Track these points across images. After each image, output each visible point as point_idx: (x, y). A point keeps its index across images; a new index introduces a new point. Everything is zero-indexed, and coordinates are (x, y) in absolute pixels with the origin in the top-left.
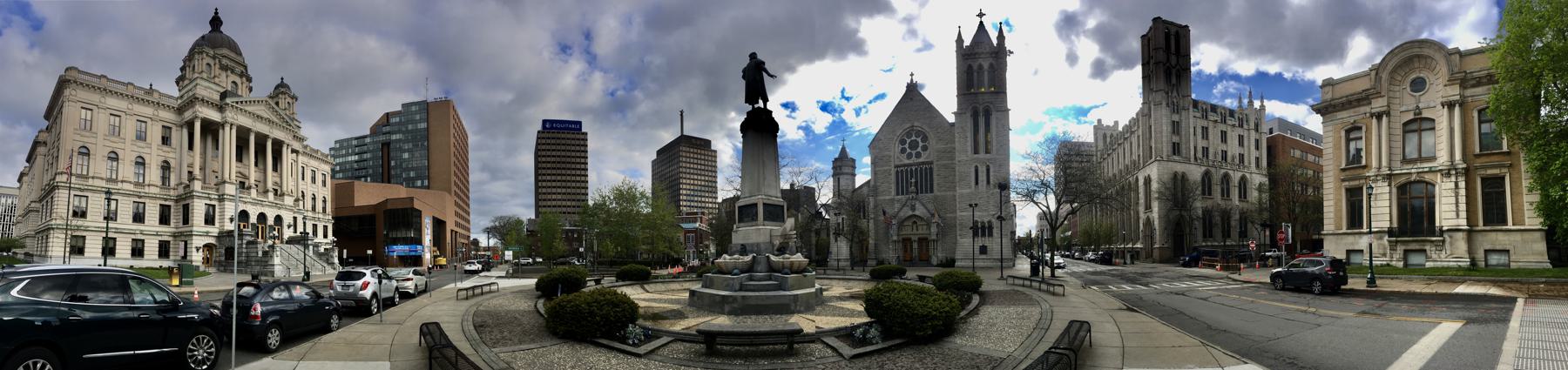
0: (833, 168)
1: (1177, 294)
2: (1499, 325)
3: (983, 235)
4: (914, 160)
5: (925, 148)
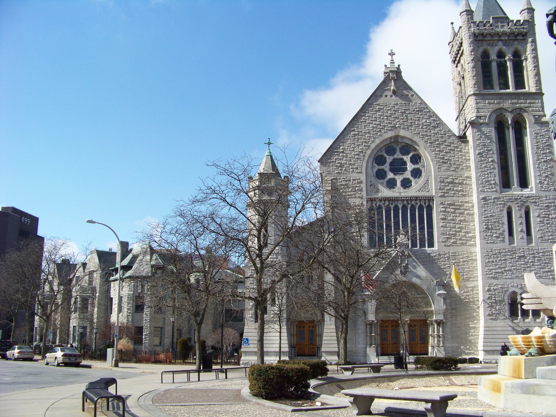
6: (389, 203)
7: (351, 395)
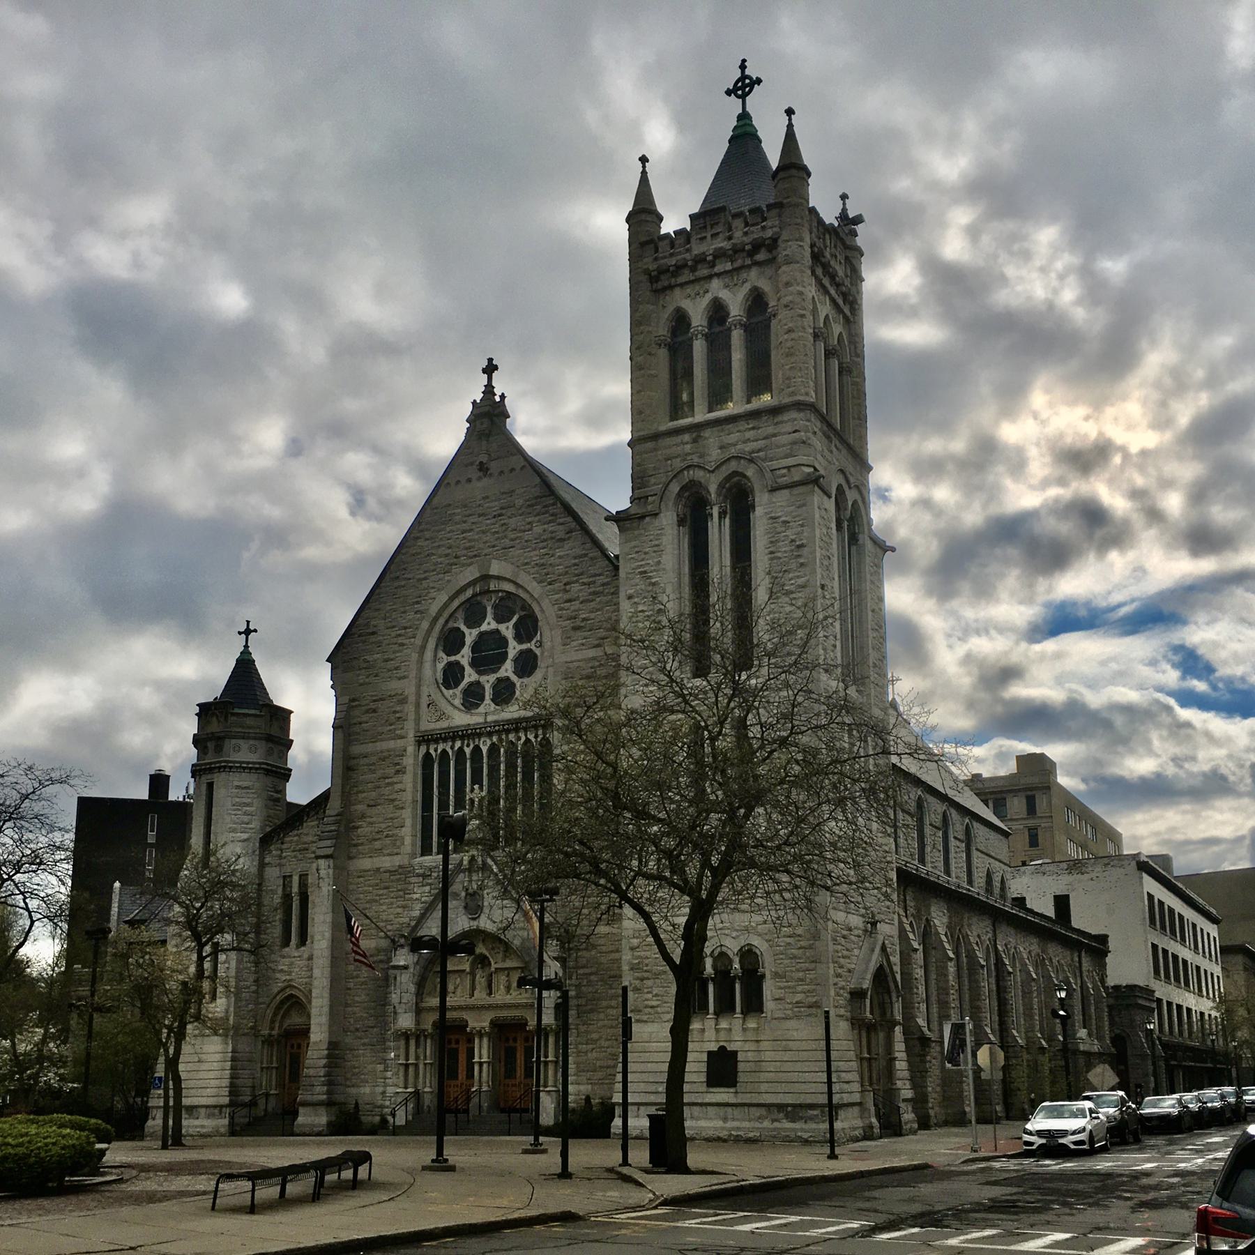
0: (197, 741)
1: (913, 1170)
2: (365, 830)
3: (725, 1007)
4: (488, 712)
5: (526, 664)
6: (463, 744)
7: (686, 1171)
